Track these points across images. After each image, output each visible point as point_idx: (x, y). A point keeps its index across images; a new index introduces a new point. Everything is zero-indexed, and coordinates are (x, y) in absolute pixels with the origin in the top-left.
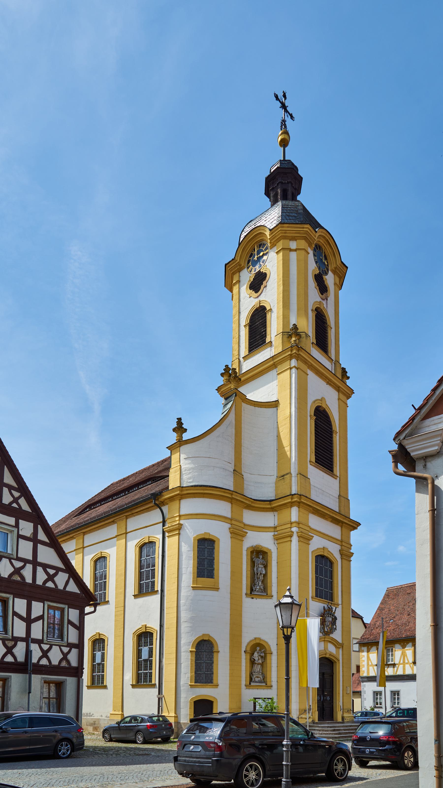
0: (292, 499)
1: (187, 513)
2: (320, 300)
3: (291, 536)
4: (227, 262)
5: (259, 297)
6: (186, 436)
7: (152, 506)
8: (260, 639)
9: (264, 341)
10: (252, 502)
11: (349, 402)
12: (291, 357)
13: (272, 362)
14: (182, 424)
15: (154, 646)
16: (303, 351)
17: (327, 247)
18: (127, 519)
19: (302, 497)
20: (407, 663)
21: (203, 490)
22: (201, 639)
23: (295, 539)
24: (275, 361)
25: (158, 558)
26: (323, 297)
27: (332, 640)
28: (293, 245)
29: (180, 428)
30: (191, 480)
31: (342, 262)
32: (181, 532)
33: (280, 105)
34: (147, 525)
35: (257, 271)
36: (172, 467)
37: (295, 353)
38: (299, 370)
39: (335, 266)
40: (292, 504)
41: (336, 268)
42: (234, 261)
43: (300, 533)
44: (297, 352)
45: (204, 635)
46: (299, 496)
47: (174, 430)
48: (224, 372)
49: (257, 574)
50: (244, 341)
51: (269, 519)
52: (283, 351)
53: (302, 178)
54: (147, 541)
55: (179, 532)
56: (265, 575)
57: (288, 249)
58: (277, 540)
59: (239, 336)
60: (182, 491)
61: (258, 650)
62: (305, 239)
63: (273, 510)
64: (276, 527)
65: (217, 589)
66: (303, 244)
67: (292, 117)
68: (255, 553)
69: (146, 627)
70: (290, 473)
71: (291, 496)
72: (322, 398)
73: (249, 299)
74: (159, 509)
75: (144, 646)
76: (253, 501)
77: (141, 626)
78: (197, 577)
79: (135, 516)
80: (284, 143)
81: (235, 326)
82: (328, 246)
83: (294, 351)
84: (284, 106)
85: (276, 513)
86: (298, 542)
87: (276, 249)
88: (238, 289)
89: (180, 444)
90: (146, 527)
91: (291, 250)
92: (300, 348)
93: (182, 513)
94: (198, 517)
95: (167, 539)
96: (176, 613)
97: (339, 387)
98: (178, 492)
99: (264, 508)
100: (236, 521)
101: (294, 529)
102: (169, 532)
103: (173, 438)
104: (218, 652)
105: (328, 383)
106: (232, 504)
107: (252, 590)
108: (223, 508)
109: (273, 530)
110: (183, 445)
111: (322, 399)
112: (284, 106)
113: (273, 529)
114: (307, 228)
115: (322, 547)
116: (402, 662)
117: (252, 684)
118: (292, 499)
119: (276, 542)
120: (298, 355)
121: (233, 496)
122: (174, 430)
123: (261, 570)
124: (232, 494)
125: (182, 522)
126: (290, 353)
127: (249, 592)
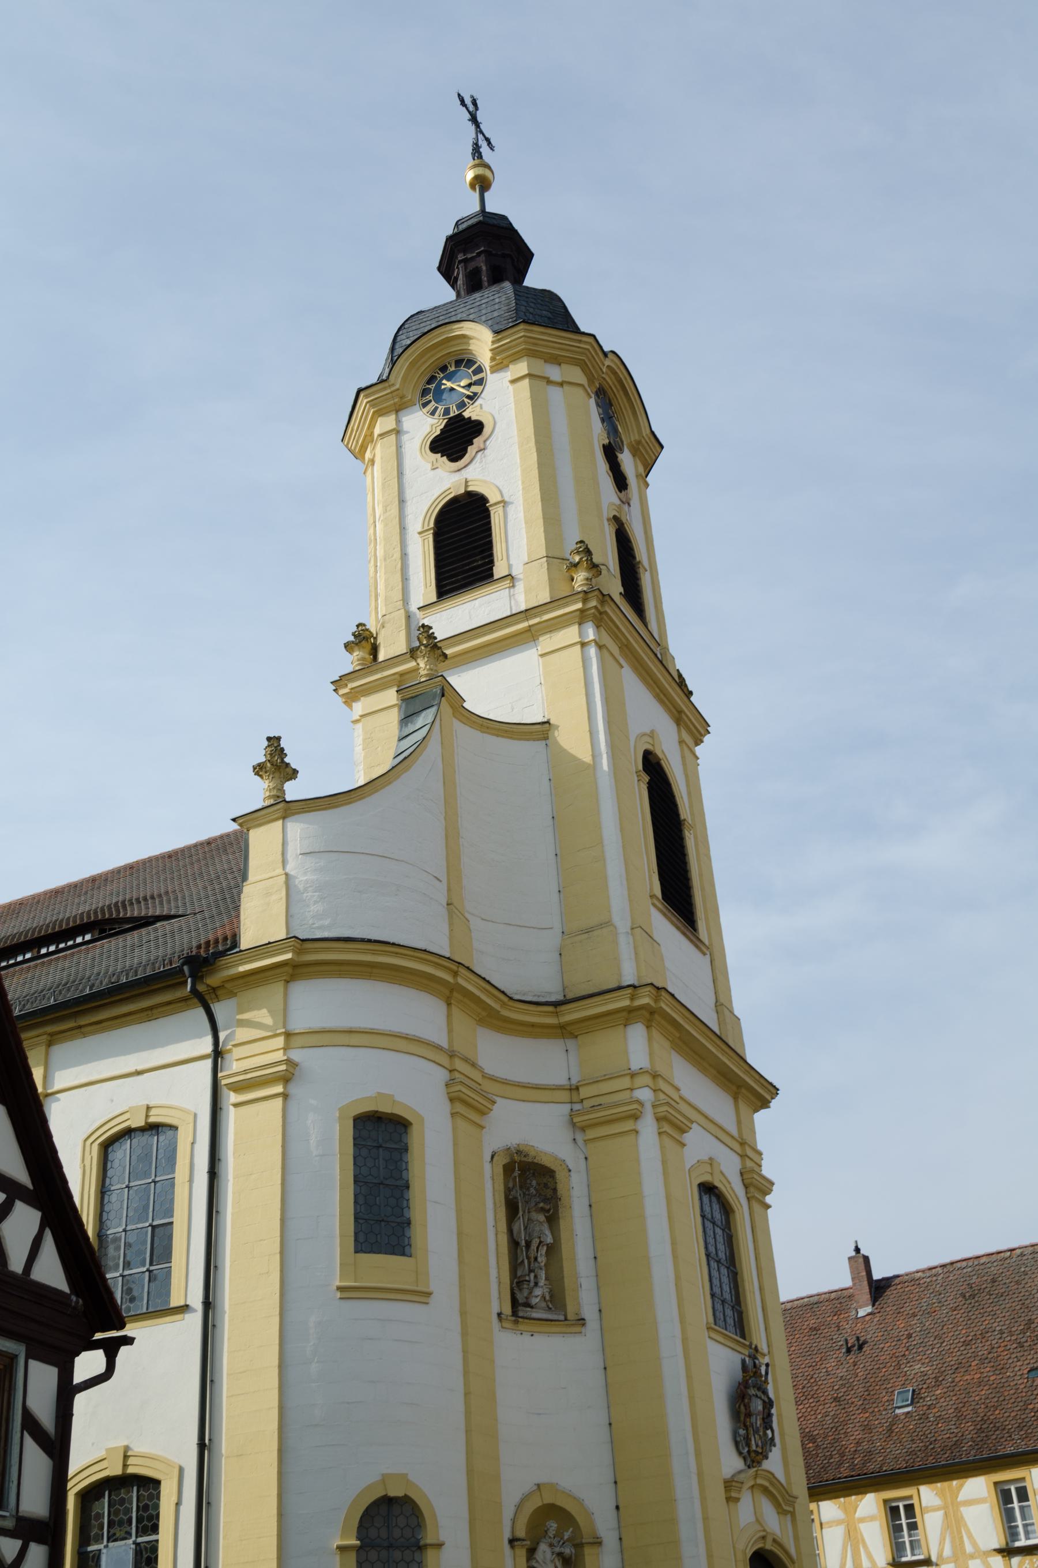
0: (632, 999)
1: (317, 1024)
2: (618, 502)
3: (636, 1117)
4: (363, 386)
5: (463, 471)
6: (293, 791)
7: (185, 1000)
8: (553, 1487)
9: (492, 575)
10: (504, 1005)
11: (699, 750)
12: (581, 618)
13: (525, 624)
14: (282, 752)
15: (164, 1537)
16: (612, 604)
17: (620, 396)
18: (50, 1044)
19: (663, 993)
20: (972, 1557)
21: (374, 952)
22: (379, 1493)
23: (648, 1127)
25: (191, 1180)
26: (622, 495)
27: (771, 1483)
28: (554, 373)
29: (276, 764)
30: (327, 922)
31: (653, 433)
32: (293, 1089)
33: (468, 116)
34: (140, 1068)
35: (452, 415)
36: (252, 876)
37: (595, 607)
38: (605, 651)
39: (637, 437)
40: (629, 1015)
41: (639, 442)
42: (386, 384)
43: (666, 1108)
44: (599, 607)
45: (385, 1479)
46: (654, 991)
47: (259, 770)
48: (352, 638)
49: (528, 1245)
50: (421, 569)
51: (548, 1062)
52: (554, 602)
53: (532, 255)
54: (138, 1122)
55: (285, 1088)
56: (553, 1250)
57: (544, 378)
58: (583, 1129)
59: (404, 556)
60: (298, 952)
61: (551, 1533)
62: (583, 365)
63: (565, 1031)
64: (577, 1088)
65: (423, 1296)
66: (576, 375)
67: (489, 143)
68: (517, 1173)
69: (126, 1457)
70: (608, 923)
71: (629, 991)
72: (652, 732)
73: (433, 472)
74: (201, 1012)
75: (112, 1538)
76: (506, 999)
77: (102, 1454)
78: (356, 1252)
79: (85, 1035)
80: (482, 184)
81: (382, 529)
82: (621, 393)
83: (593, 603)
84: (474, 119)
85: (571, 1043)
86: (656, 1136)
87: (508, 375)
88: (394, 448)
89: (286, 810)
90: (138, 1073)
91: (549, 382)
92: (607, 598)
93: (298, 1024)
94: (355, 1039)
95: (231, 1118)
96: (276, 1392)
97: (680, 712)
98: (289, 956)
99: (533, 1025)
100: (466, 1060)
101: (645, 1095)
102: (238, 1087)
103: (256, 792)
104: (440, 1545)
105: (657, 697)
106: (449, 1004)
107: (515, 1303)
108: (422, 1014)
109: (565, 1096)
110: (294, 814)
111: (652, 735)
112: (474, 119)
113: (567, 1093)
114: (586, 343)
115: (706, 1158)
116: (947, 1552)
118: (632, 999)
119: (580, 1137)
120: (601, 613)
121: (460, 981)
122: (259, 770)
123: (541, 1232)
124: (455, 974)
125: (296, 1055)
126: (579, 605)
127: (507, 1310)
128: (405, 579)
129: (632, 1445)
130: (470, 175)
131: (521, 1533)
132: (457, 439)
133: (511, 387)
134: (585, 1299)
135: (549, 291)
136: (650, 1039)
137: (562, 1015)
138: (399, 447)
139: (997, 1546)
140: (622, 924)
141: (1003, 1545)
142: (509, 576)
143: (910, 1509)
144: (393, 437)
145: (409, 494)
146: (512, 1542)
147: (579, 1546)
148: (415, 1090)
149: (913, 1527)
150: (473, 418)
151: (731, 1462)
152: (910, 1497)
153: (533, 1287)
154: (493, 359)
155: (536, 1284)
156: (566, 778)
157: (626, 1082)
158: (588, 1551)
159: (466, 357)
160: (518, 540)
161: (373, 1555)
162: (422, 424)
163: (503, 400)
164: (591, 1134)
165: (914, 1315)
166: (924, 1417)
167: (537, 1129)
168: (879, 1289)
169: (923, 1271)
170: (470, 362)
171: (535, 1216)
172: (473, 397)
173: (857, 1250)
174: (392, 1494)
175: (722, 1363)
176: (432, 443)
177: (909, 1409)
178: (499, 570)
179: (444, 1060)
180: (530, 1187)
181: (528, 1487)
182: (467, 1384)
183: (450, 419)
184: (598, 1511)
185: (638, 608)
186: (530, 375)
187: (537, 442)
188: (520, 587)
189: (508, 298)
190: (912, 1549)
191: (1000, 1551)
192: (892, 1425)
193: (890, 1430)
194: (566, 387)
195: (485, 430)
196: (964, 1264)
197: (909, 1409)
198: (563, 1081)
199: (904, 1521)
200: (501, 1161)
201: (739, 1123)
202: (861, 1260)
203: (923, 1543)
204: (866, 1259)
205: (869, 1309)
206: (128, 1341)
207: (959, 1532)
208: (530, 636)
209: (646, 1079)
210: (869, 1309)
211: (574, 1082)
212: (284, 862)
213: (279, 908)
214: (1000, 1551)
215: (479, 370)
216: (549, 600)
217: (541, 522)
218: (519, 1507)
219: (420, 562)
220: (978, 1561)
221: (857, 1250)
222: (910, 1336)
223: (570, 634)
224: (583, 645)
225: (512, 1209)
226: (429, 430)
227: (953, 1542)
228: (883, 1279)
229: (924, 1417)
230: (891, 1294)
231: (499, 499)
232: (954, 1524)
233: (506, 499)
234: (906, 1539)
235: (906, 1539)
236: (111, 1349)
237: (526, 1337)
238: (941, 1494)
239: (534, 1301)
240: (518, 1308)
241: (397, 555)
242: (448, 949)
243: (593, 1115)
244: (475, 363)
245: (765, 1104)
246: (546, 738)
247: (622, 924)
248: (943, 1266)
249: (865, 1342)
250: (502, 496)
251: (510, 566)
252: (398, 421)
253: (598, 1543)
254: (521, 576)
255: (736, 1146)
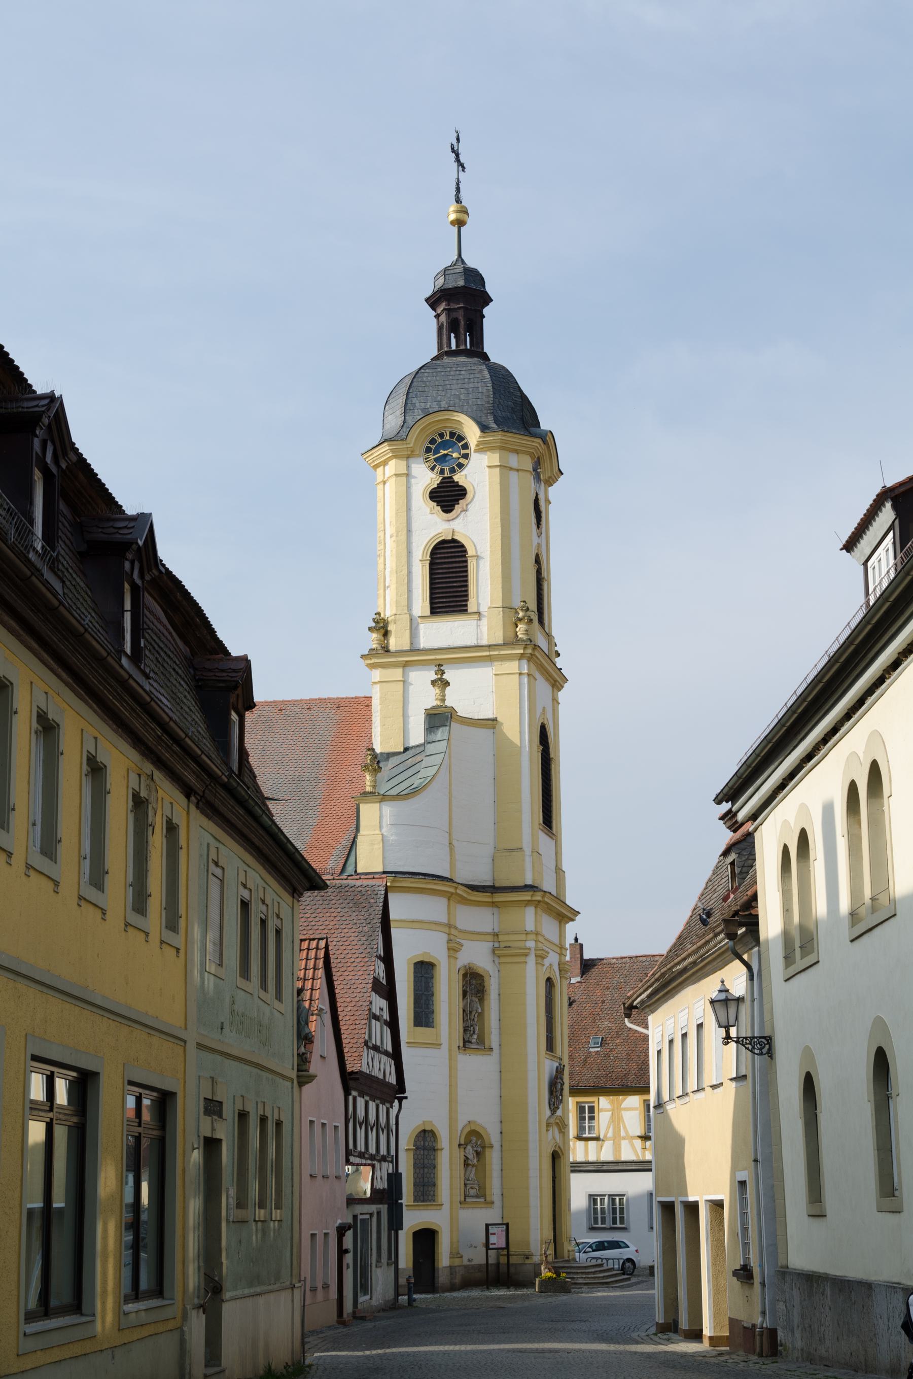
3: (526, 955)
12: (521, 657)
13: (487, 653)
20: (624, 1138)
23: (531, 960)
24: (492, 653)
40: (528, 903)
49: (471, 1012)
51: (477, 918)
52: (506, 644)
56: (481, 1015)
59: (409, 573)
62: (531, 455)
65: (438, 1045)
70: (520, 849)
85: (496, 910)
101: (531, 944)
107: (465, 1042)
109: (491, 938)
116: (610, 1134)
117: (468, 1200)
119: (497, 961)
121: (458, 891)
126: (521, 651)
127: (461, 1045)
128: (410, 591)
129: (509, 1106)
130: (453, 217)
131: (462, 1142)
132: (448, 496)
133: (487, 469)
134: (493, 1039)
135: (482, 279)
136: (536, 913)
137: (489, 891)
138: (408, 487)
139: (639, 1134)
140: (527, 850)
141: (643, 1134)
142: (479, 613)
143: (592, 1110)
144: (404, 478)
145: (415, 526)
146: (460, 1145)
147: (484, 1147)
148: (433, 947)
149: (592, 1118)
150: (460, 484)
151: (548, 1113)
152: (593, 1102)
153: (472, 1036)
154: (477, 445)
155: (474, 1032)
156: (502, 751)
157: (523, 937)
158: (487, 1150)
159: (458, 432)
160: (485, 584)
161: (418, 1152)
162: (426, 478)
163: (480, 473)
164: (503, 960)
165: (608, 988)
166: (607, 1056)
167: (478, 955)
168: (587, 966)
169: (617, 959)
170: (461, 438)
171: (474, 998)
172: (461, 466)
173: (576, 940)
174: (427, 1129)
175: (549, 1066)
176: (431, 493)
177: (599, 1049)
178: (472, 606)
179: (447, 930)
180: (473, 984)
181: (466, 1122)
182: (450, 1081)
183: (444, 478)
184: (493, 1136)
185: (541, 621)
186: (500, 466)
187: (501, 519)
188: (484, 622)
189: (488, 391)
190: (589, 1130)
191: (640, 1137)
192: (586, 1058)
193: (585, 1061)
194: (520, 473)
195: (468, 495)
196: (644, 959)
197: (599, 1049)
198: (490, 930)
199: (587, 1115)
200: (462, 972)
201: (560, 936)
202: (578, 947)
203: (596, 1128)
204: (581, 946)
205: (579, 979)
206: (406, 1098)
207: (619, 1124)
208: (490, 659)
209: (533, 937)
210: (579, 979)
211: (496, 931)
212: (381, 827)
213: (378, 852)
214: (640, 1137)
215: (466, 446)
216: (501, 642)
217: (500, 579)
218: (462, 1131)
219: (420, 582)
220: (627, 1141)
221: (576, 940)
222: (603, 1002)
223: (513, 666)
224: (520, 674)
225: (465, 994)
226: (429, 481)
227: (614, 1129)
228: (590, 960)
229: (607, 1056)
230: (595, 971)
231: (474, 554)
232: (616, 1120)
233: (479, 554)
234: (587, 1125)
235: (587, 1125)
236: (400, 1100)
237: (468, 1056)
238: (612, 1103)
239: (474, 1041)
240: (466, 1043)
241: (405, 572)
242: (447, 866)
243: (503, 949)
244: (463, 439)
245: (573, 920)
246: (494, 728)
247: (527, 850)
248: (631, 958)
249: (574, 1001)
250: (476, 552)
251: (478, 604)
252: (408, 467)
253: (491, 1146)
254: (485, 614)
255: (558, 950)
